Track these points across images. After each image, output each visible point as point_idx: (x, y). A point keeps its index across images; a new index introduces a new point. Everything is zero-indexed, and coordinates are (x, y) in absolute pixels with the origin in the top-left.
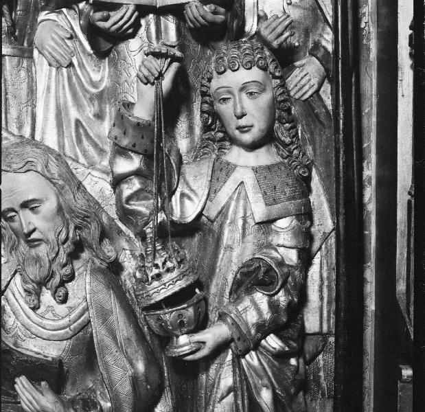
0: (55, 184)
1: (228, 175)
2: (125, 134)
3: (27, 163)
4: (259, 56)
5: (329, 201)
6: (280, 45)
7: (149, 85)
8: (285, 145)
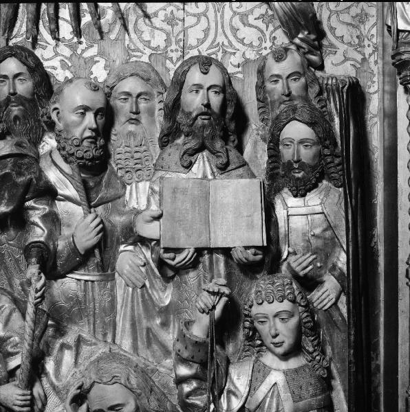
0: (133, 392)
1: (265, 377)
2: (186, 348)
3: (114, 377)
4: (289, 291)
5: (344, 391)
6: (306, 275)
7: (205, 314)
8: (310, 353)
